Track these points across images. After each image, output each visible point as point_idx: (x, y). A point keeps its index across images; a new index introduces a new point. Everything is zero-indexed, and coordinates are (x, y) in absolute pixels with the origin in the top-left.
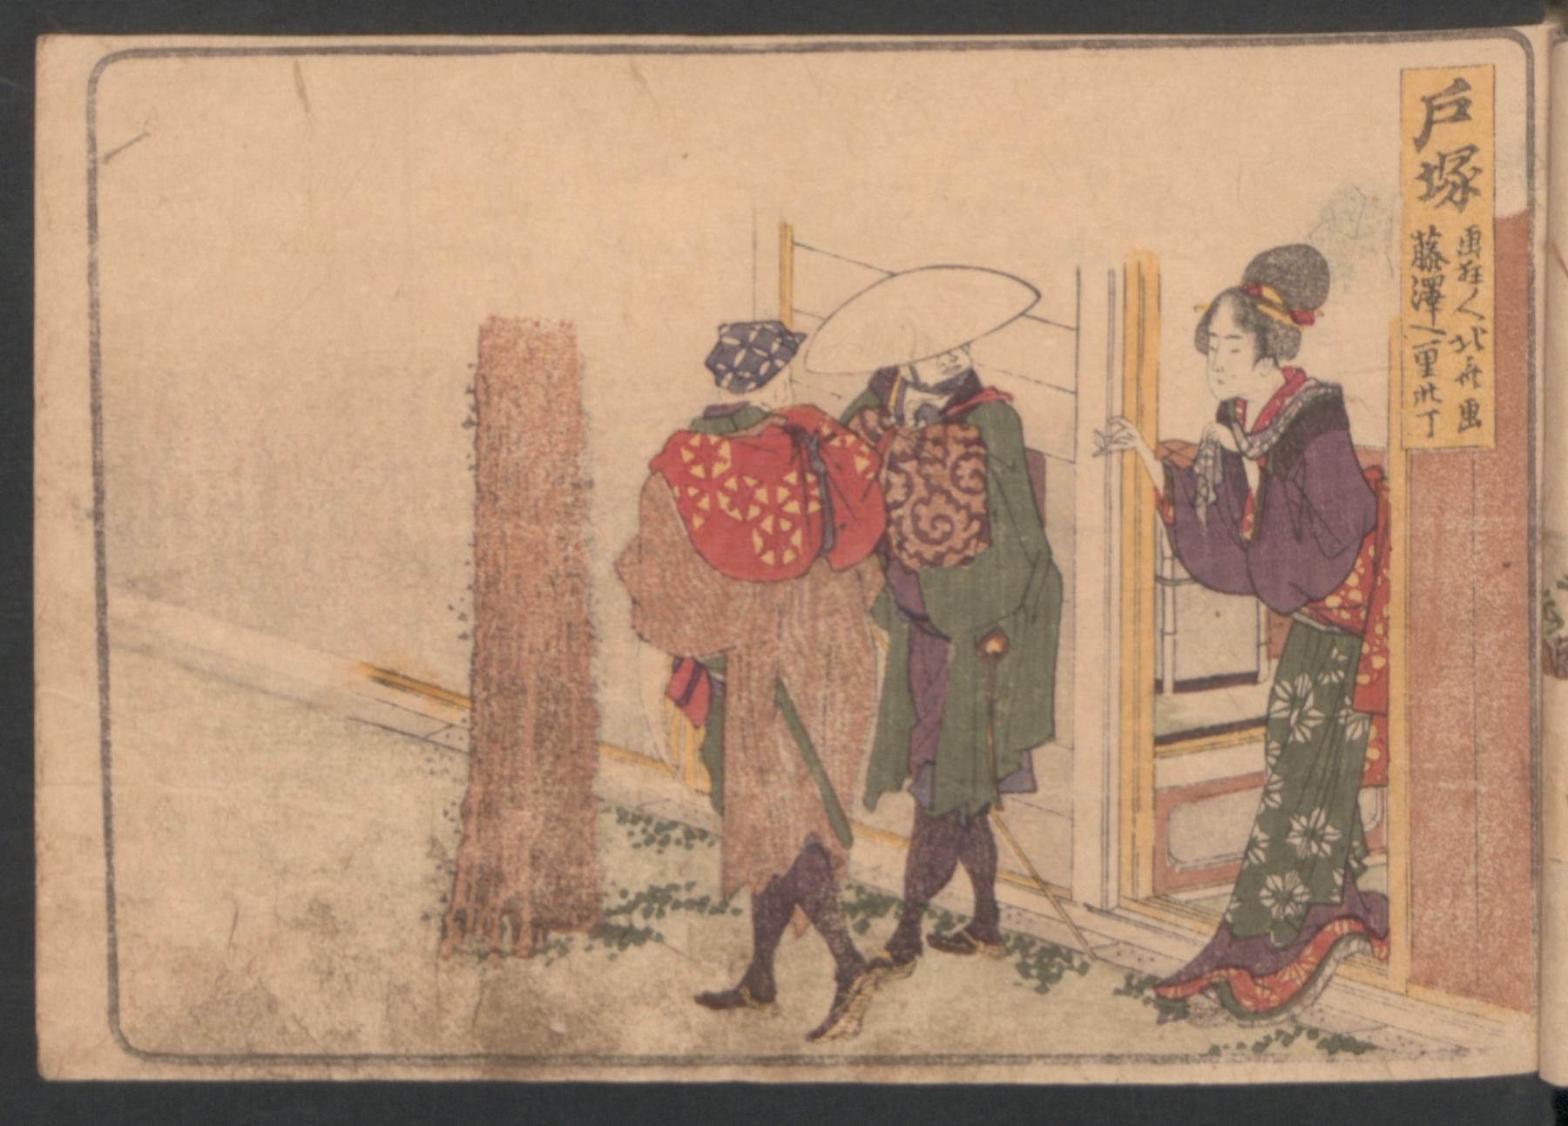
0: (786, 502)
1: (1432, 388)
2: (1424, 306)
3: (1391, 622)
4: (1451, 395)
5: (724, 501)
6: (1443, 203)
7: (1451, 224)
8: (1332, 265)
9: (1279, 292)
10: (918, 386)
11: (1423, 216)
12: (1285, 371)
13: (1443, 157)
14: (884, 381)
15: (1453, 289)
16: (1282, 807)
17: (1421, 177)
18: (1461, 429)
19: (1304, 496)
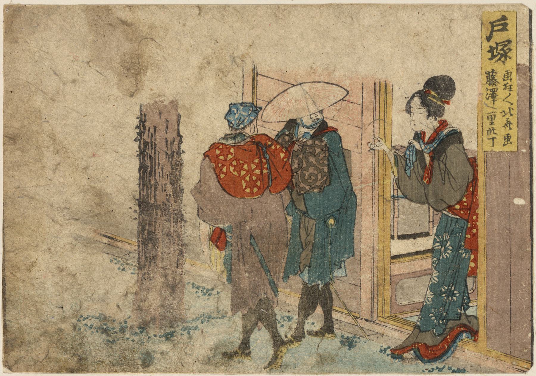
0: (245, 170)
1: (493, 129)
2: (490, 99)
3: (479, 216)
4: (501, 132)
5: (232, 169)
6: (498, 61)
7: (500, 69)
8: (454, 78)
9: (437, 91)
10: (303, 125)
11: (490, 66)
12: (439, 122)
13: (497, 44)
14: (292, 124)
15: (501, 93)
16: (438, 283)
17: (489, 51)
18: (504, 145)
19: (446, 167)
